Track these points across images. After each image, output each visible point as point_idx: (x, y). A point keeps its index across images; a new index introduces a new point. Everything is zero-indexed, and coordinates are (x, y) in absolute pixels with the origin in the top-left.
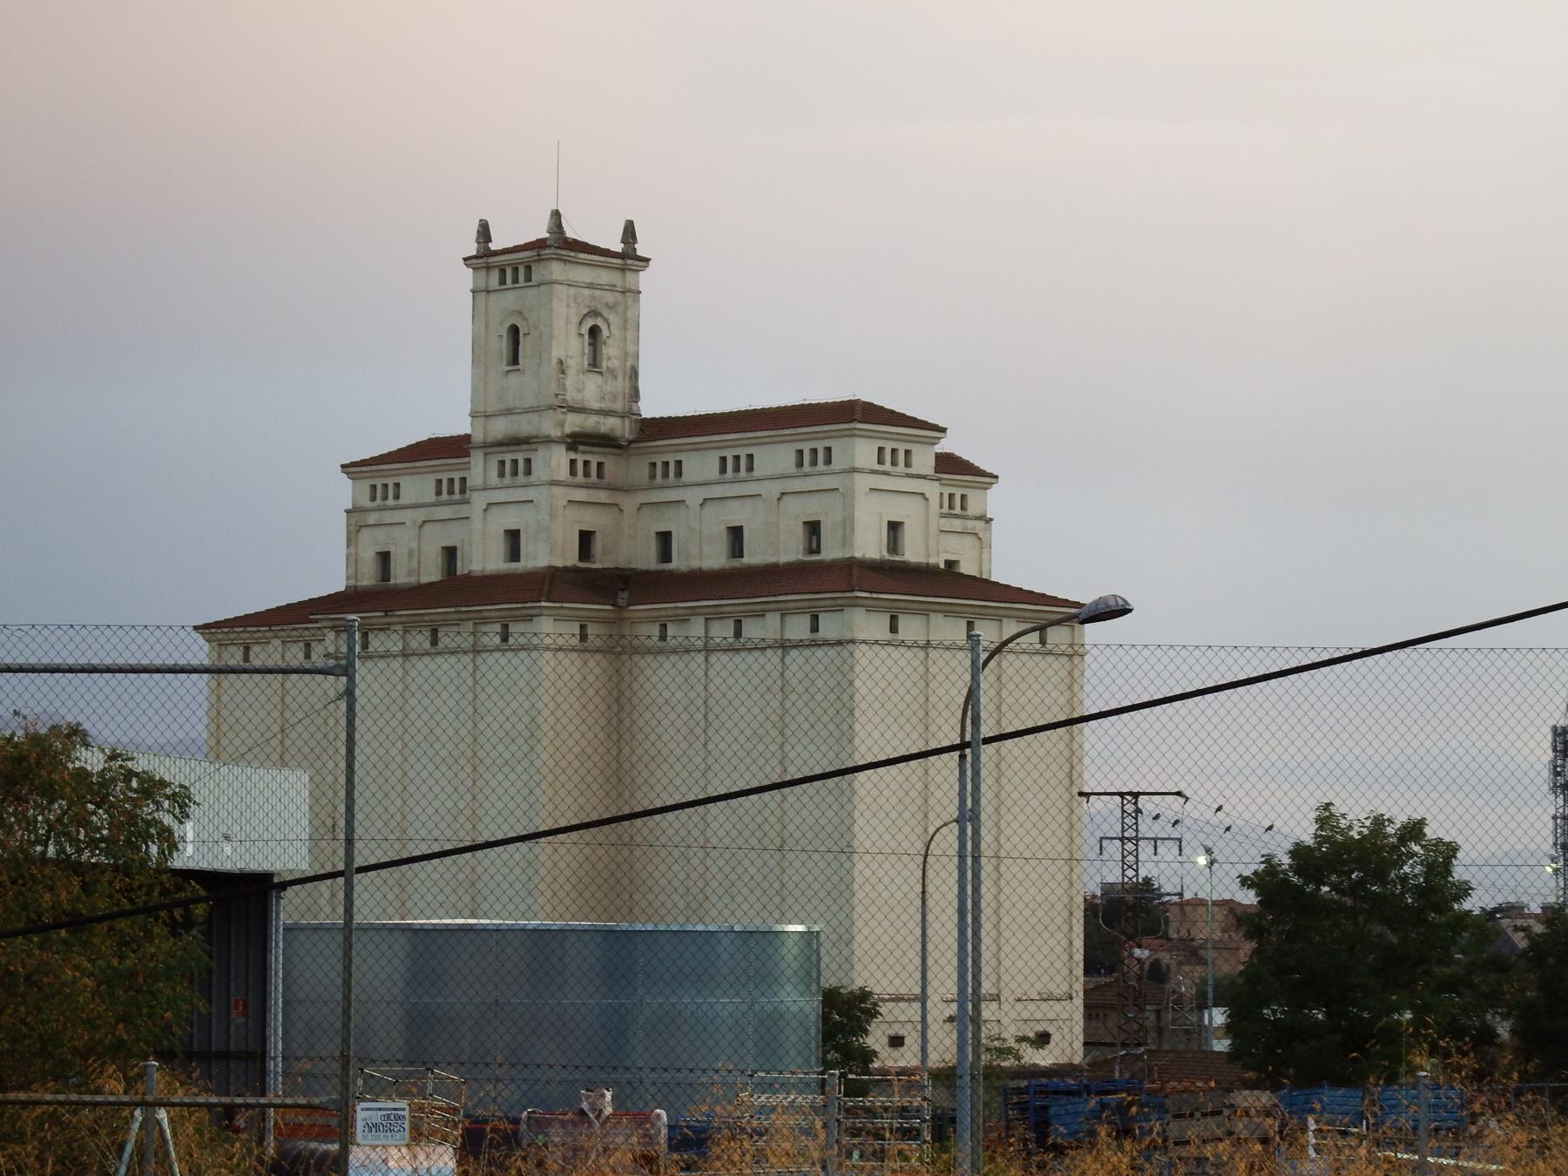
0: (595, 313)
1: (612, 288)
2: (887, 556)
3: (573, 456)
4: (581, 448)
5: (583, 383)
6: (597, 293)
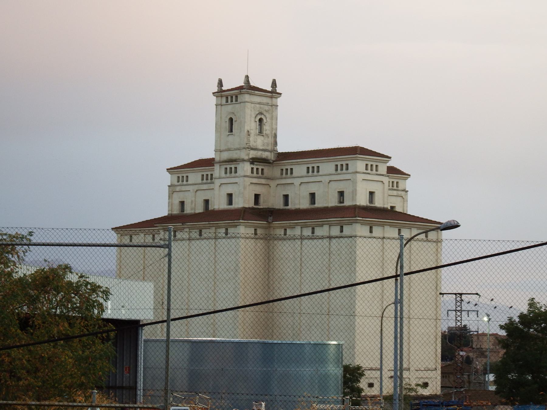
0: (261, 113)
1: (267, 104)
2: (369, 204)
3: (252, 166)
4: (255, 163)
5: (256, 139)
6: (262, 106)
